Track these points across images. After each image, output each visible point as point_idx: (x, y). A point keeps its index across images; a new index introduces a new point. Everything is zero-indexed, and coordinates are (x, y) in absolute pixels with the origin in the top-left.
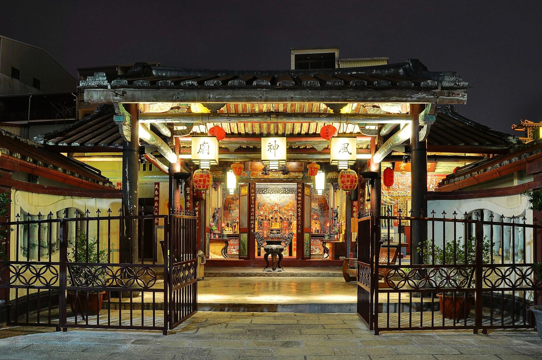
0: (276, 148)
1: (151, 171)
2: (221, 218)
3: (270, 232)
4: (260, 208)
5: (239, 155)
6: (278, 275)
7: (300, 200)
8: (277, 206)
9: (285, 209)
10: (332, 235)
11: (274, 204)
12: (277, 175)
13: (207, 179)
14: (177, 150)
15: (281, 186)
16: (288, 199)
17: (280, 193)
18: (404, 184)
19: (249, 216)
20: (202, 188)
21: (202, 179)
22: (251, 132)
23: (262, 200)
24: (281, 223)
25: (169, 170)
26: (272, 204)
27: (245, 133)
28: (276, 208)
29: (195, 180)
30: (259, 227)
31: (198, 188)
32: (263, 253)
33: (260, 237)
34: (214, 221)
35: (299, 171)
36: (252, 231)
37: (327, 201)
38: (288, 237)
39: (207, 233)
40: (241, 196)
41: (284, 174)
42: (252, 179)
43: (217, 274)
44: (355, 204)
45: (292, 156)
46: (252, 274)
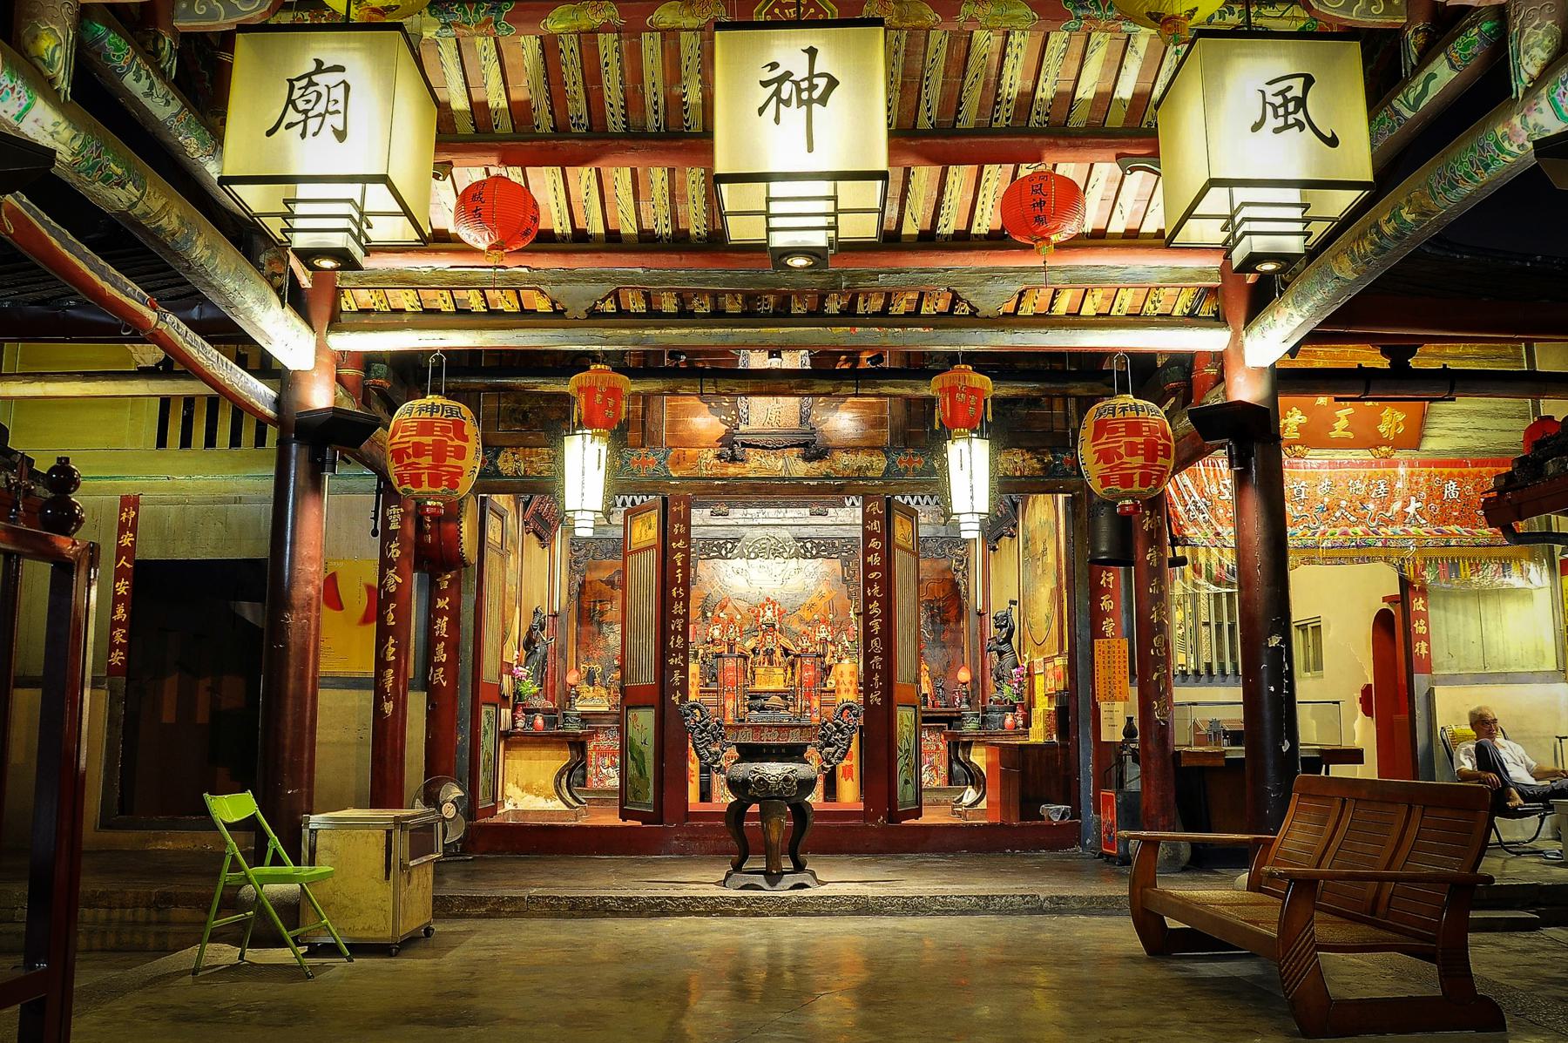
0: (816, 94)
1: (260, 450)
2: (562, 652)
3: (748, 706)
4: (709, 614)
5: (608, 332)
6: (796, 909)
7: (875, 569)
8: (771, 607)
9: (801, 620)
10: (994, 715)
11: (763, 601)
12: (781, 463)
13: (449, 443)
14: (322, 312)
15: (795, 517)
16: (811, 582)
17: (785, 555)
18: (1303, 496)
19: (664, 634)
20: (426, 487)
21: (427, 440)
22: (664, 228)
23: (717, 587)
24: (789, 669)
25: (278, 404)
26: (755, 601)
27: (641, 231)
28: (769, 614)
29: (394, 447)
30: (707, 685)
31: (409, 487)
32: (723, 798)
33: (707, 725)
34: (531, 661)
35: (868, 447)
36: (676, 698)
37: (958, 584)
38: (837, 725)
39: (484, 709)
40: (632, 553)
41: (807, 459)
42: (675, 479)
43: (501, 901)
44: (1108, 583)
45: (858, 335)
46: (670, 905)
